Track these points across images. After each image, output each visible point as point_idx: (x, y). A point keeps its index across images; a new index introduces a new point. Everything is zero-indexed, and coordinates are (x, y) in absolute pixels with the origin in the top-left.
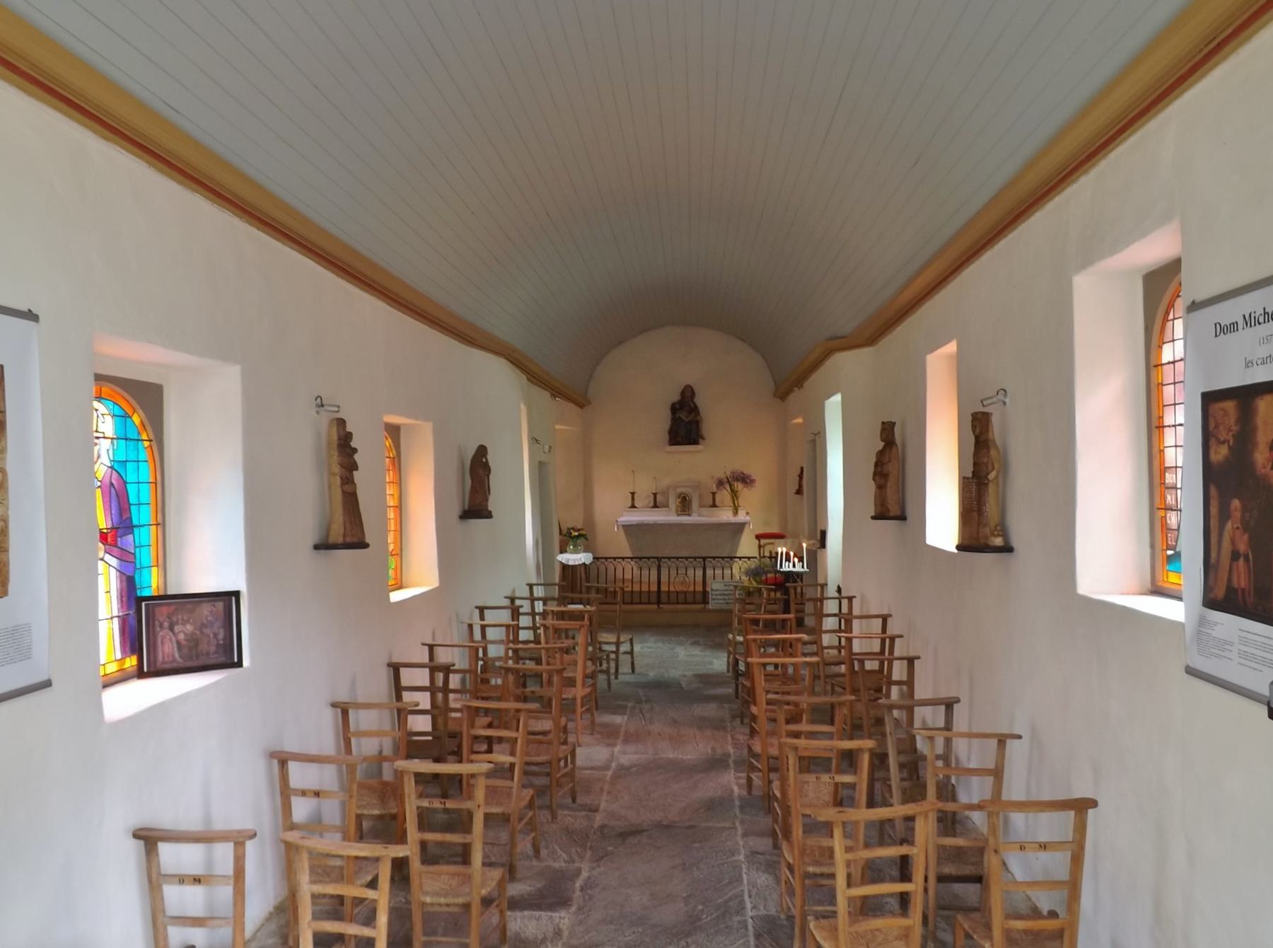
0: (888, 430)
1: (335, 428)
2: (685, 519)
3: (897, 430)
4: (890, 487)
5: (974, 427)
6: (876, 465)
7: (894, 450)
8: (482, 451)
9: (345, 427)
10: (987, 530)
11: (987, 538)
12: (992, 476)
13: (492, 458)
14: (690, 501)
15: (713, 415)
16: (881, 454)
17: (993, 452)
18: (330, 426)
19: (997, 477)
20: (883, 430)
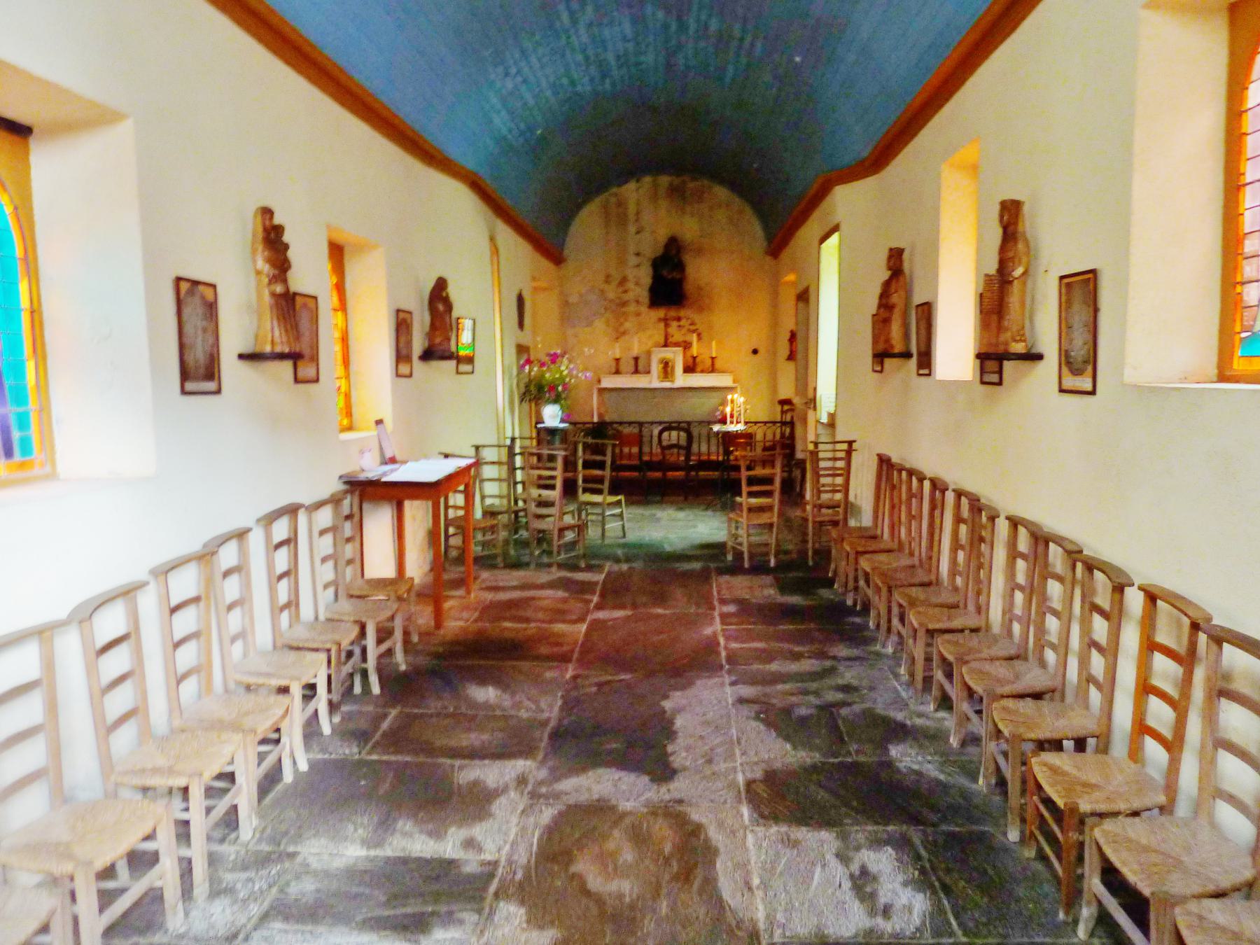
0: (896, 256)
1: (259, 219)
2: (667, 385)
3: (906, 256)
4: (899, 331)
5: (1001, 217)
6: (882, 296)
7: (901, 278)
8: (441, 285)
9: (271, 218)
10: (1008, 334)
11: (1007, 344)
12: (1018, 272)
13: (453, 292)
14: (673, 368)
15: (699, 271)
16: (887, 285)
17: (1020, 246)
18: (255, 216)
19: (1025, 273)
20: (890, 258)
